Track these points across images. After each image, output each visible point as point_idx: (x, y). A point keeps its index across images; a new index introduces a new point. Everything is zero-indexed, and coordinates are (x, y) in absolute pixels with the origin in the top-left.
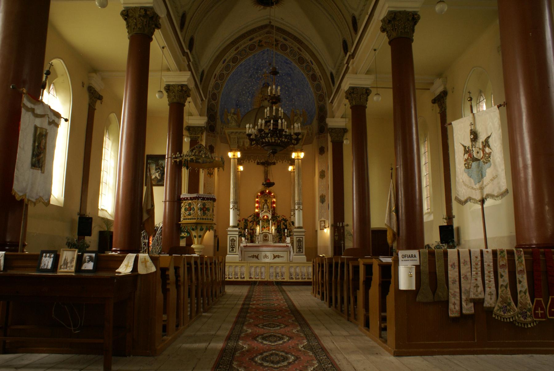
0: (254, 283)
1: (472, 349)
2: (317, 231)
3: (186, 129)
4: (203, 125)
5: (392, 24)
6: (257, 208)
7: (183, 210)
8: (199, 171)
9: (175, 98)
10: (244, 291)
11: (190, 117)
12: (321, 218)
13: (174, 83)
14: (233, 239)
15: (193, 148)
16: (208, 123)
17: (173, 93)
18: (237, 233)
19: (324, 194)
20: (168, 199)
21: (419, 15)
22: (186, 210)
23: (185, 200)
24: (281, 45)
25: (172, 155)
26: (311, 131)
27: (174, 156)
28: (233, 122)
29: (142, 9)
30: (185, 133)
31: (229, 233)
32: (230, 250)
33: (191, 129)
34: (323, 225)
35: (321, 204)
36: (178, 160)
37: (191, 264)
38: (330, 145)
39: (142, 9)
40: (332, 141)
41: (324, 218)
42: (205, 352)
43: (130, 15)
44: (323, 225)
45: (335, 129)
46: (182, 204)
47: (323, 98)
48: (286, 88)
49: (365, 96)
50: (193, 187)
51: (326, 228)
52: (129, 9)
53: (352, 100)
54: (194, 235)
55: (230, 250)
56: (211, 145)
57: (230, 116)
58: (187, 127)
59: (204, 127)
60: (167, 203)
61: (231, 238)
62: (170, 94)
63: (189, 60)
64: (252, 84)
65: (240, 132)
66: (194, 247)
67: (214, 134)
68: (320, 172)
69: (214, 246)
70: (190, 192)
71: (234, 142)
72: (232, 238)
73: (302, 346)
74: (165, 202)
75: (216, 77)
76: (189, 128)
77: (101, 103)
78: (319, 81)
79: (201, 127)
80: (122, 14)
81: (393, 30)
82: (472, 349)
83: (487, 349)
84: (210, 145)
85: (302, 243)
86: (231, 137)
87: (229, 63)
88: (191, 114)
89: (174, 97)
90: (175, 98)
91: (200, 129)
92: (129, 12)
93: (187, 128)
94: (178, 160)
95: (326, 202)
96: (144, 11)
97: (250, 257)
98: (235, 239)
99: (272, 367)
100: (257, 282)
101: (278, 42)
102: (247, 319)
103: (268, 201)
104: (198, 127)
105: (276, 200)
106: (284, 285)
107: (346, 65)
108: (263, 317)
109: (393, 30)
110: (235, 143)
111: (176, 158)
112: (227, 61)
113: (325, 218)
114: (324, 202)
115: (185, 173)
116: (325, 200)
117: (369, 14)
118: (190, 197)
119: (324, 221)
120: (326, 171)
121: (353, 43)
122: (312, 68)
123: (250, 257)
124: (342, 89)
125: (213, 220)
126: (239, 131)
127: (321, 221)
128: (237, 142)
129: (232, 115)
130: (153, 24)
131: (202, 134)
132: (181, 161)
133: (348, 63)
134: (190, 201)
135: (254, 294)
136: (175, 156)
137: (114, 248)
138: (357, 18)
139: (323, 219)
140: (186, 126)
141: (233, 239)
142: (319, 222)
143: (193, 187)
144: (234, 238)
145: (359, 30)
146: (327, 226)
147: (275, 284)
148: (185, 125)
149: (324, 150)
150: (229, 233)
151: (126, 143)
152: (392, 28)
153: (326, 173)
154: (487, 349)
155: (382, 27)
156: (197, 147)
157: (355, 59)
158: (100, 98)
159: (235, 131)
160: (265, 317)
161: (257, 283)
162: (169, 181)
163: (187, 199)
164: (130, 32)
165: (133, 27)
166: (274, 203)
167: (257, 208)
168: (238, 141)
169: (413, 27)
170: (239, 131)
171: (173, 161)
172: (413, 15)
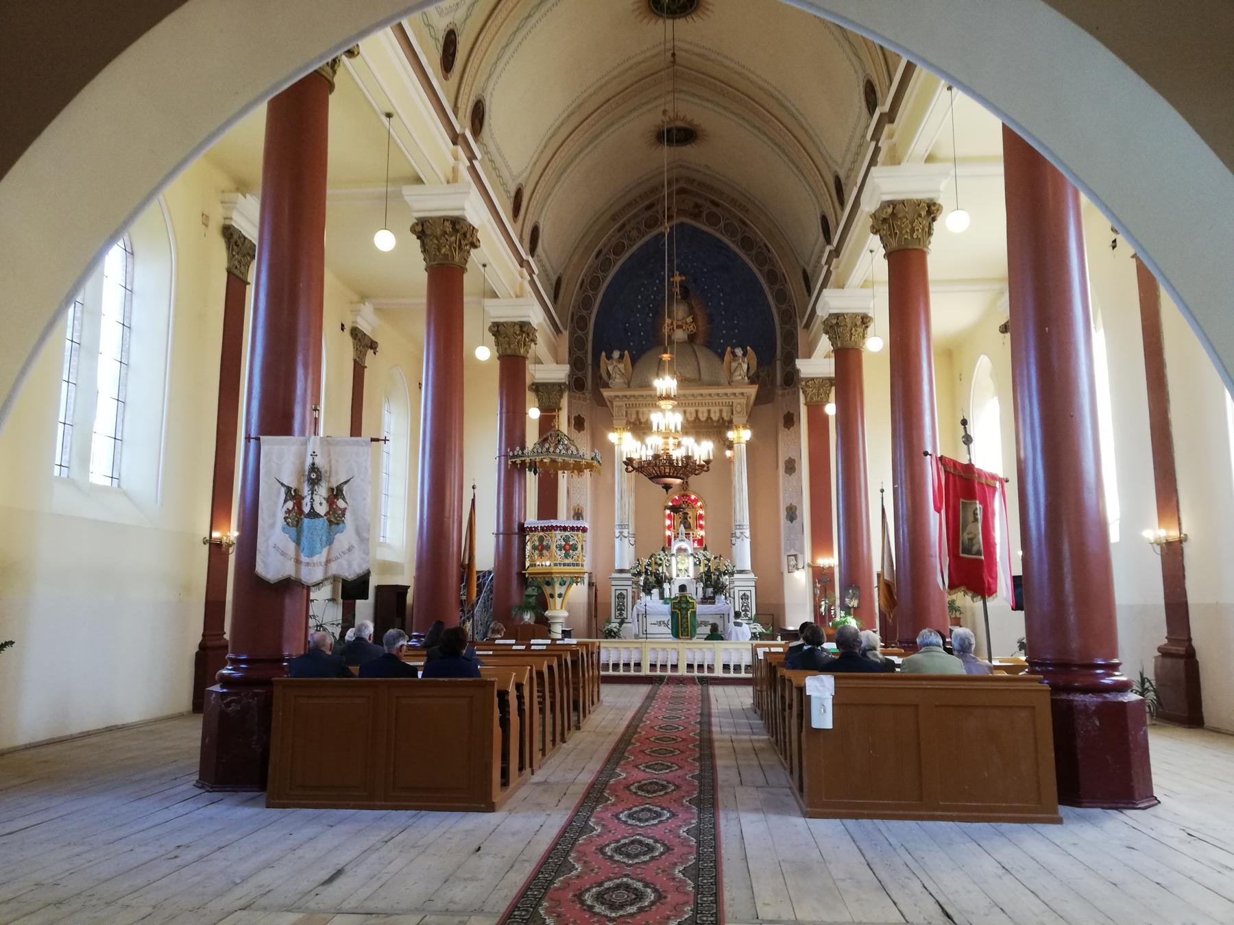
0: (659, 680)
1: (917, 813)
2: (782, 573)
3: (532, 389)
4: (563, 381)
5: (889, 225)
6: (669, 527)
7: (528, 547)
8: (556, 475)
9: (510, 346)
10: (635, 696)
11: (538, 366)
12: (789, 551)
13: (506, 320)
14: (621, 594)
15: (545, 436)
16: (571, 375)
17: (505, 337)
18: (630, 583)
19: (794, 504)
20: (501, 530)
21: (940, 205)
22: (534, 548)
23: (532, 531)
24: (707, 215)
25: (507, 452)
26: (770, 378)
27: (511, 454)
28: (618, 376)
29: (448, 220)
30: (530, 397)
31: (614, 583)
32: (617, 615)
33: (540, 388)
34: (793, 562)
35: (789, 522)
36: (518, 461)
37: (543, 673)
38: (803, 411)
39: (448, 220)
40: (806, 404)
41: (795, 550)
42: (557, 806)
43: (428, 232)
44: (793, 562)
45: (813, 379)
46: (528, 538)
47: (791, 317)
48: (721, 295)
49: (860, 330)
50: (548, 506)
51: (798, 569)
52: (426, 221)
53: (836, 338)
54: (549, 593)
55: (617, 615)
56: (579, 415)
57: (611, 365)
58: (533, 384)
59: (565, 383)
60: (501, 536)
61: (618, 592)
62: (501, 339)
63: (531, 272)
64: (655, 289)
65: (631, 396)
66: (550, 615)
67: (584, 393)
68: (786, 461)
69: (589, 603)
70: (541, 516)
71: (620, 414)
72: (619, 592)
73: (688, 799)
74: (497, 534)
75: (584, 285)
76: (538, 388)
77: (375, 353)
78: (783, 285)
79: (560, 385)
80: (413, 230)
81: (890, 235)
82: (917, 813)
83: (939, 813)
84: (577, 415)
85: (749, 601)
86: (614, 403)
87: (607, 256)
88: (538, 361)
89: (507, 346)
90: (510, 346)
91: (557, 388)
92: (425, 226)
93: (534, 387)
94: (518, 461)
95: (798, 519)
96: (451, 223)
97: (654, 624)
98: (625, 594)
99: (637, 825)
100: (664, 677)
101: (701, 209)
102: (626, 754)
103: (690, 514)
104: (554, 384)
105: (705, 512)
106: (712, 684)
107: (826, 268)
108: (676, 740)
109: (890, 235)
110: (622, 416)
111: (514, 456)
112: (604, 252)
113: (798, 551)
114: (796, 519)
115: (532, 480)
116: (796, 515)
117: (858, 185)
118: (541, 527)
119: (795, 556)
120: (796, 459)
121: (838, 224)
122: (769, 258)
123: (654, 624)
124: (818, 316)
125: (582, 566)
126: (628, 393)
127: (788, 556)
128: (625, 414)
129: (615, 363)
130: (466, 245)
131: (561, 396)
132: (523, 462)
133: (829, 262)
134: (541, 534)
135: (653, 704)
136: (513, 454)
137: (416, 632)
138: (843, 181)
139: (793, 552)
140: (531, 383)
141: (621, 594)
142: (786, 557)
143: (548, 506)
144: (623, 592)
145: (848, 201)
146: (800, 566)
147: (697, 680)
148: (528, 381)
149: (792, 419)
150: (614, 583)
151: (431, 456)
152: (889, 233)
153: (797, 462)
154: (939, 813)
155: (873, 227)
156: (551, 435)
157: (840, 257)
158: (373, 346)
159: (620, 394)
160: (654, 753)
161: (665, 680)
162: (504, 497)
163: (536, 529)
164: (428, 260)
165: (434, 253)
166: (701, 517)
167: (669, 527)
168: (626, 412)
169: (930, 228)
170: (628, 393)
171: (510, 463)
172: (929, 206)
